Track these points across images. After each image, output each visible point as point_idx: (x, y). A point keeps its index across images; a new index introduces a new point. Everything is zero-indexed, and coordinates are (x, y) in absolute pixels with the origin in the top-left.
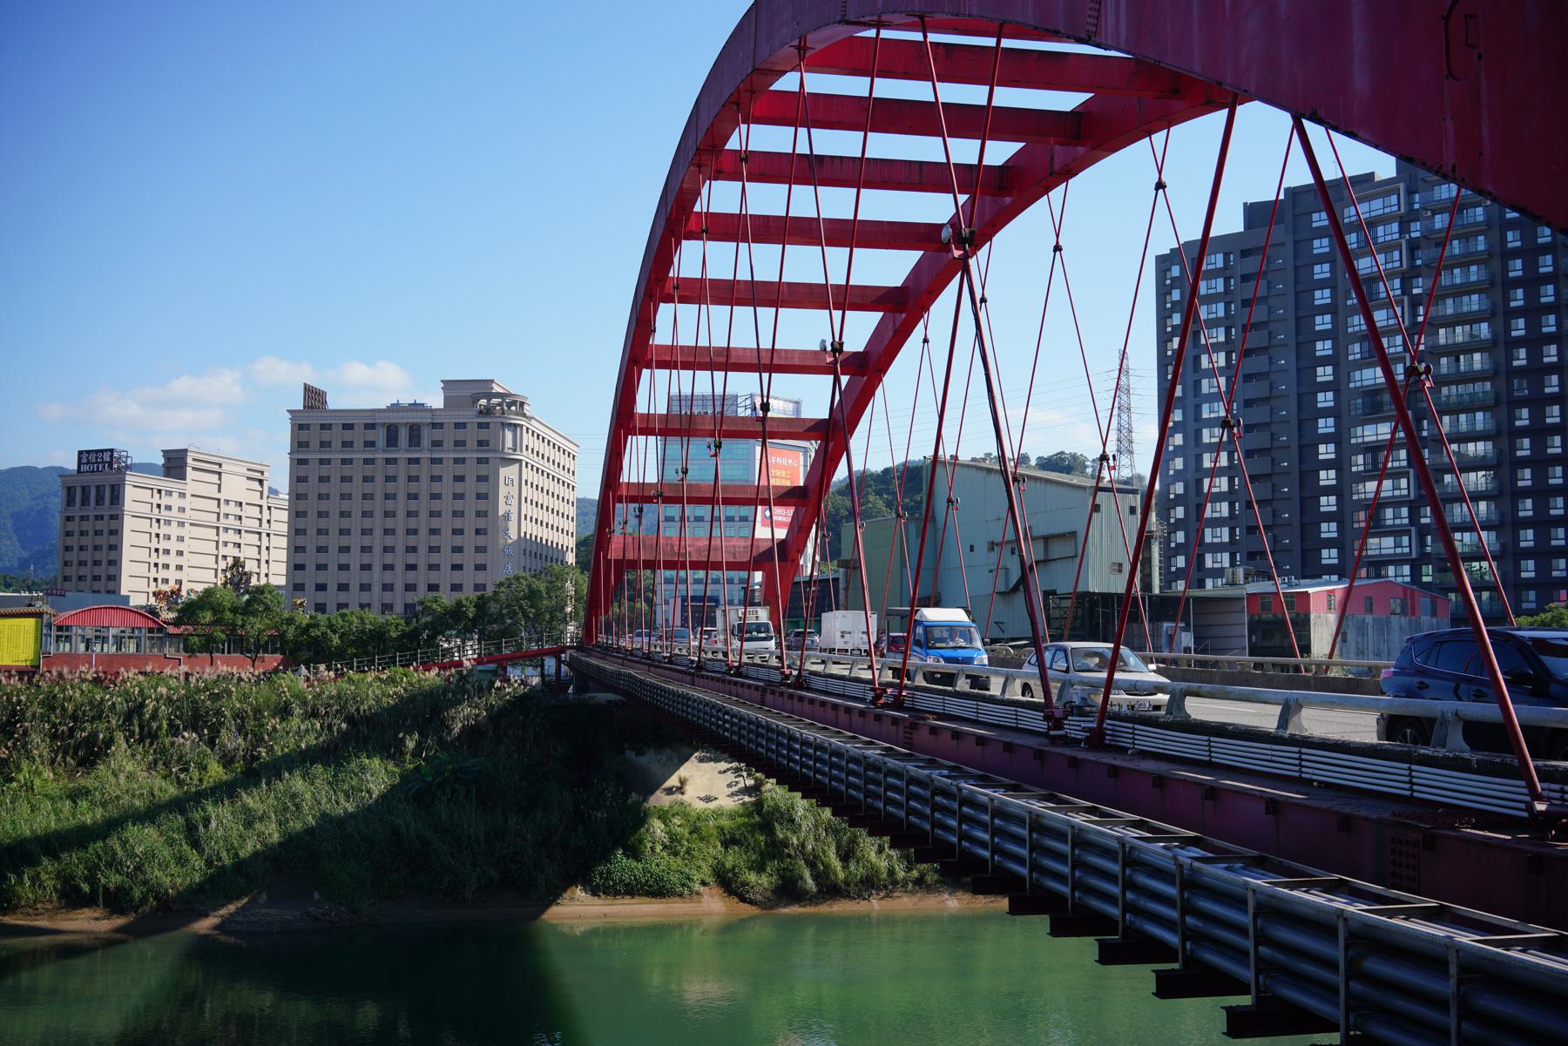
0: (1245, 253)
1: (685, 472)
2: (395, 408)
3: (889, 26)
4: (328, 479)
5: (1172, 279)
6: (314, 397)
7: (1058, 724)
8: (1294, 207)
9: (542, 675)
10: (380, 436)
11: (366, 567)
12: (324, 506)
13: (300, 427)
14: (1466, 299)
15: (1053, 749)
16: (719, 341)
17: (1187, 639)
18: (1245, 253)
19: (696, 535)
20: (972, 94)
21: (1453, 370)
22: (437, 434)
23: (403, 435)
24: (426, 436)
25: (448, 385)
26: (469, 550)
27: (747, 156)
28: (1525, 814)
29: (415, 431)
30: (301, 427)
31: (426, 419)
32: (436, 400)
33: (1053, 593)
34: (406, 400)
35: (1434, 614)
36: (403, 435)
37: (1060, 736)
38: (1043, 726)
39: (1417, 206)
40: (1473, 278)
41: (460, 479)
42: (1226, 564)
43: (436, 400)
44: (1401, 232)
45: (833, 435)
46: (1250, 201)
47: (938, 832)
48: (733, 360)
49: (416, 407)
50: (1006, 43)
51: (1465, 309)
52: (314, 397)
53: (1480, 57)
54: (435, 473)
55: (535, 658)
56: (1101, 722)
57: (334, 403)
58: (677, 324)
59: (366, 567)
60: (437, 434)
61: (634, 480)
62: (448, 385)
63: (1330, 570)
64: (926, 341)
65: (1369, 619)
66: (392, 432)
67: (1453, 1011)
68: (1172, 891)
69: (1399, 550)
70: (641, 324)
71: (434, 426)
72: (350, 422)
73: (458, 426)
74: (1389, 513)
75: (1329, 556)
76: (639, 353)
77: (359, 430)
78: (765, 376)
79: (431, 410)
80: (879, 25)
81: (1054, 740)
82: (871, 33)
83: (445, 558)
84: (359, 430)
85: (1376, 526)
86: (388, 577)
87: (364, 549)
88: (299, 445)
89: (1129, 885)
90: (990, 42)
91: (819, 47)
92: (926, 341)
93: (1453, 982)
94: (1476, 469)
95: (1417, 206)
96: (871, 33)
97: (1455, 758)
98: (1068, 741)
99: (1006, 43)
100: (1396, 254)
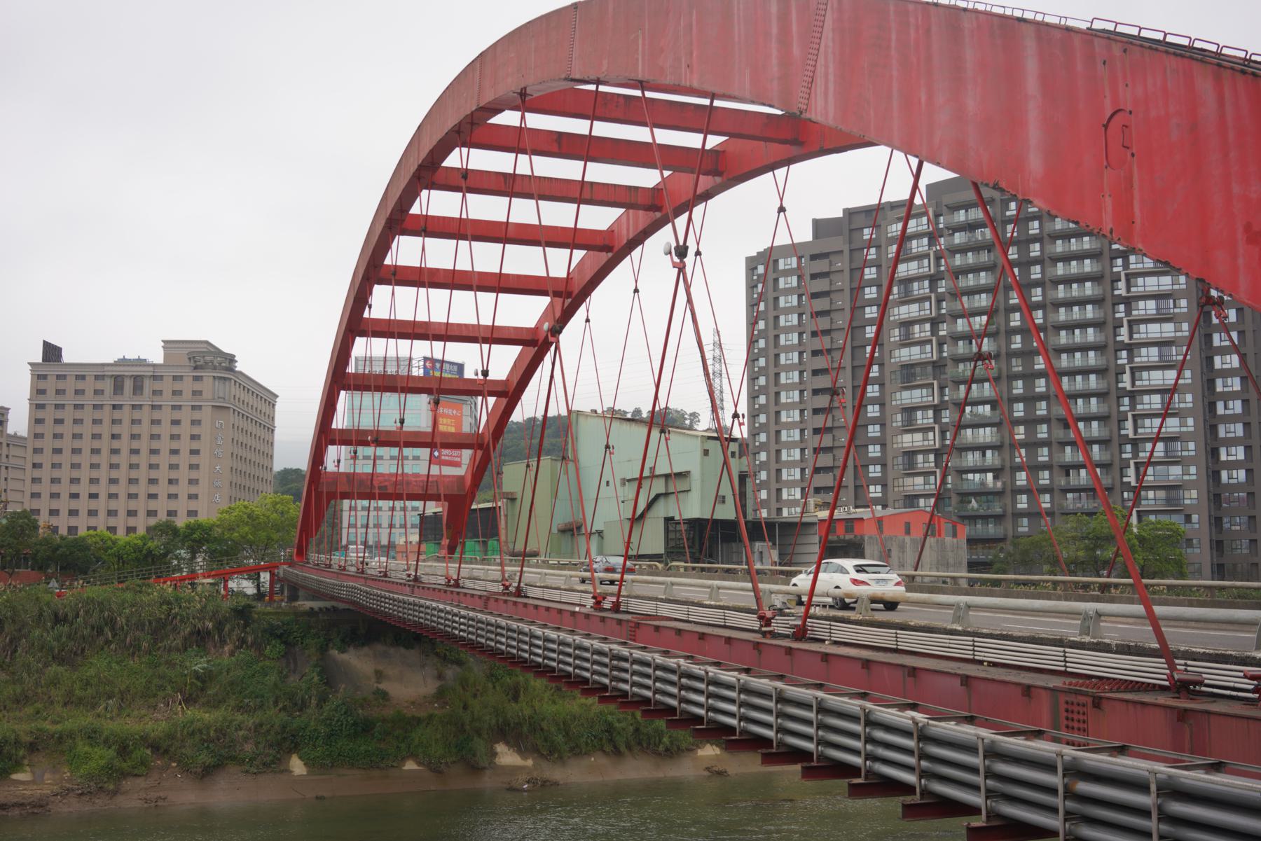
0: (813, 257)
1: (402, 421)
2: (123, 362)
3: (605, 83)
4: (100, 422)
5: (759, 276)
6: (52, 352)
7: (768, 622)
8: (850, 223)
9: (258, 587)
10: (108, 386)
11: (93, 496)
12: (77, 444)
13: (39, 375)
14: (977, 297)
15: (764, 641)
16: (486, 321)
17: (775, 554)
18: (813, 257)
19: (387, 467)
20: (638, 134)
21: (967, 351)
22: (158, 386)
23: (128, 385)
24: (148, 386)
25: (168, 344)
26: (183, 482)
27: (465, 173)
28: (1167, 683)
29: (138, 381)
30: (39, 377)
31: (148, 372)
32: (156, 356)
33: (672, 519)
34: (131, 356)
35: (955, 535)
36: (128, 385)
37: (770, 632)
38: (756, 625)
39: (941, 226)
40: (983, 281)
41: (176, 422)
42: (798, 496)
43: (156, 356)
44: (930, 245)
45: (511, 392)
46: (819, 217)
47: (683, 705)
48: (417, 331)
49: (140, 362)
50: (649, 94)
51: (976, 305)
52: (52, 352)
53: (1133, 155)
54: (155, 418)
55: (254, 574)
56: (804, 622)
57: (67, 358)
58: (386, 302)
59: (93, 496)
60: (158, 386)
61: (340, 427)
62: (168, 344)
63: (876, 501)
64: (588, 320)
65: (907, 539)
66: (118, 382)
67: (1154, 816)
68: (910, 743)
69: (927, 487)
70: (359, 298)
71: (155, 377)
72: (82, 372)
73: (175, 378)
74: (920, 458)
75: (875, 491)
76: (356, 323)
77: (90, 380)
78: (485, 347)
79: (154, 365)
80: (598, 82)
81: (764, 634)
82: (592, 87)
83: (162, 489)
84: (90, 380)
85: (911, 470)
86: (93, 504)
87: (92, 481)
88: (38, 392)
89: (870, 740)
90: (638, 93)
91: (536, 95)
92: (588, 320)
93: (1154, 795)
94: (984, 426)
95: (941, 226)
96: (592, 87)
97: (1098, 643)
98: (774, 635)
99: (649, 94)
100: (926, 261)
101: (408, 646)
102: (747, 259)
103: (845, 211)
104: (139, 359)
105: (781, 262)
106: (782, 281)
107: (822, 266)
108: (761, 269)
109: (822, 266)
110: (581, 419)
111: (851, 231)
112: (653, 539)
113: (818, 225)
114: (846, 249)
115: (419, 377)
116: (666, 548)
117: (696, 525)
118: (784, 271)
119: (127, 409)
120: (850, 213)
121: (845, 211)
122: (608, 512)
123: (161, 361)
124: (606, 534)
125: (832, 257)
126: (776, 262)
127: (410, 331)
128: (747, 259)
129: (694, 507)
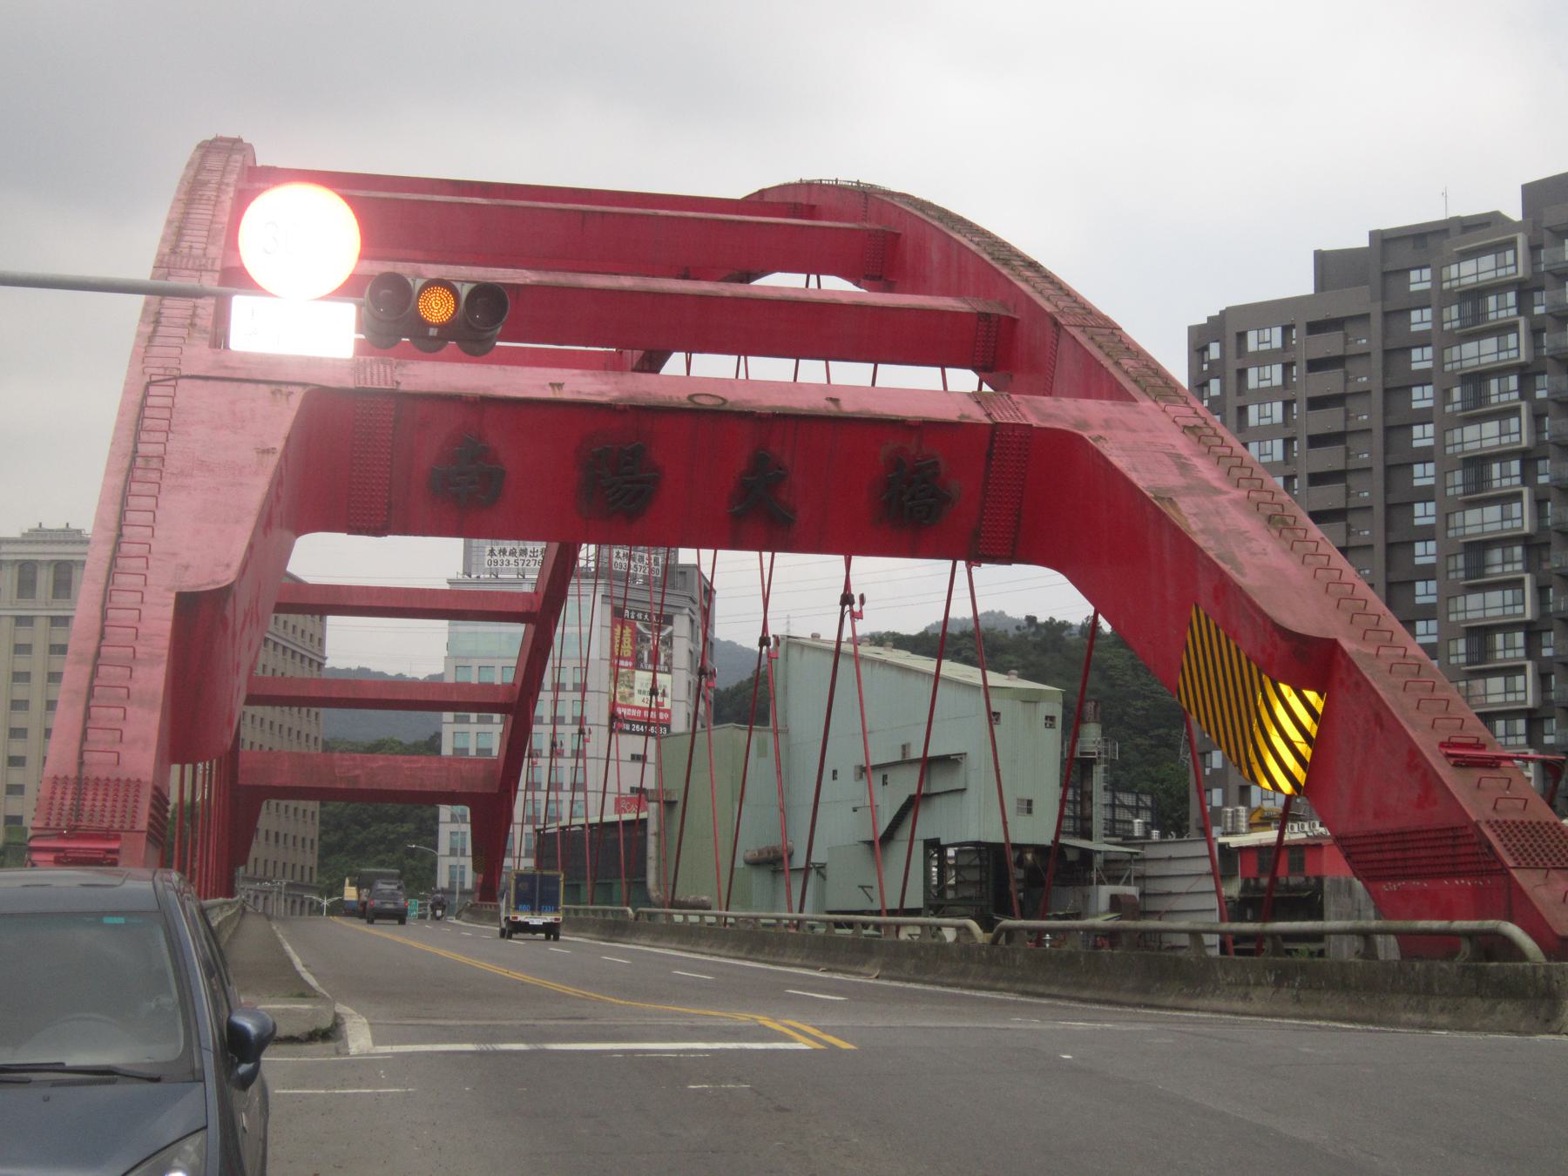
0: (1314, 328)
2: (38, 536)
18: (1314, 328)
23: (45, 579)
34: (54, 523)
36: (45, 579)
46: (1327, 246)
66: (27, 574)
101: (415, 745)
102: (1191, 329)
103: (1374, 235)
104: (67, 530)
105: (1252, 337)
106: (1252, 374)
107: (1330, 344)
108: (1214, 351)
109: (1330, 344)
110: (794, 653)
111: (1385, 274)
112: (904, 877)
113: (1326, 263)
114: (1376, 311)
115: (575, 558)
116: (926, 899)
117: (992, 858)
118: (1258, 353)
119: (41, 625)
120: (1384, 241)
121: (1374, 235)
122: (842, 825)
123: (332, 620)
124: (829, 872)
125: (1350, 328)
126: (1242, 336)
127: (474, 559)
128: (1191, 329)
129: (969, 820)
